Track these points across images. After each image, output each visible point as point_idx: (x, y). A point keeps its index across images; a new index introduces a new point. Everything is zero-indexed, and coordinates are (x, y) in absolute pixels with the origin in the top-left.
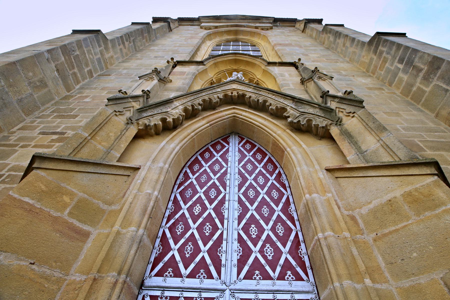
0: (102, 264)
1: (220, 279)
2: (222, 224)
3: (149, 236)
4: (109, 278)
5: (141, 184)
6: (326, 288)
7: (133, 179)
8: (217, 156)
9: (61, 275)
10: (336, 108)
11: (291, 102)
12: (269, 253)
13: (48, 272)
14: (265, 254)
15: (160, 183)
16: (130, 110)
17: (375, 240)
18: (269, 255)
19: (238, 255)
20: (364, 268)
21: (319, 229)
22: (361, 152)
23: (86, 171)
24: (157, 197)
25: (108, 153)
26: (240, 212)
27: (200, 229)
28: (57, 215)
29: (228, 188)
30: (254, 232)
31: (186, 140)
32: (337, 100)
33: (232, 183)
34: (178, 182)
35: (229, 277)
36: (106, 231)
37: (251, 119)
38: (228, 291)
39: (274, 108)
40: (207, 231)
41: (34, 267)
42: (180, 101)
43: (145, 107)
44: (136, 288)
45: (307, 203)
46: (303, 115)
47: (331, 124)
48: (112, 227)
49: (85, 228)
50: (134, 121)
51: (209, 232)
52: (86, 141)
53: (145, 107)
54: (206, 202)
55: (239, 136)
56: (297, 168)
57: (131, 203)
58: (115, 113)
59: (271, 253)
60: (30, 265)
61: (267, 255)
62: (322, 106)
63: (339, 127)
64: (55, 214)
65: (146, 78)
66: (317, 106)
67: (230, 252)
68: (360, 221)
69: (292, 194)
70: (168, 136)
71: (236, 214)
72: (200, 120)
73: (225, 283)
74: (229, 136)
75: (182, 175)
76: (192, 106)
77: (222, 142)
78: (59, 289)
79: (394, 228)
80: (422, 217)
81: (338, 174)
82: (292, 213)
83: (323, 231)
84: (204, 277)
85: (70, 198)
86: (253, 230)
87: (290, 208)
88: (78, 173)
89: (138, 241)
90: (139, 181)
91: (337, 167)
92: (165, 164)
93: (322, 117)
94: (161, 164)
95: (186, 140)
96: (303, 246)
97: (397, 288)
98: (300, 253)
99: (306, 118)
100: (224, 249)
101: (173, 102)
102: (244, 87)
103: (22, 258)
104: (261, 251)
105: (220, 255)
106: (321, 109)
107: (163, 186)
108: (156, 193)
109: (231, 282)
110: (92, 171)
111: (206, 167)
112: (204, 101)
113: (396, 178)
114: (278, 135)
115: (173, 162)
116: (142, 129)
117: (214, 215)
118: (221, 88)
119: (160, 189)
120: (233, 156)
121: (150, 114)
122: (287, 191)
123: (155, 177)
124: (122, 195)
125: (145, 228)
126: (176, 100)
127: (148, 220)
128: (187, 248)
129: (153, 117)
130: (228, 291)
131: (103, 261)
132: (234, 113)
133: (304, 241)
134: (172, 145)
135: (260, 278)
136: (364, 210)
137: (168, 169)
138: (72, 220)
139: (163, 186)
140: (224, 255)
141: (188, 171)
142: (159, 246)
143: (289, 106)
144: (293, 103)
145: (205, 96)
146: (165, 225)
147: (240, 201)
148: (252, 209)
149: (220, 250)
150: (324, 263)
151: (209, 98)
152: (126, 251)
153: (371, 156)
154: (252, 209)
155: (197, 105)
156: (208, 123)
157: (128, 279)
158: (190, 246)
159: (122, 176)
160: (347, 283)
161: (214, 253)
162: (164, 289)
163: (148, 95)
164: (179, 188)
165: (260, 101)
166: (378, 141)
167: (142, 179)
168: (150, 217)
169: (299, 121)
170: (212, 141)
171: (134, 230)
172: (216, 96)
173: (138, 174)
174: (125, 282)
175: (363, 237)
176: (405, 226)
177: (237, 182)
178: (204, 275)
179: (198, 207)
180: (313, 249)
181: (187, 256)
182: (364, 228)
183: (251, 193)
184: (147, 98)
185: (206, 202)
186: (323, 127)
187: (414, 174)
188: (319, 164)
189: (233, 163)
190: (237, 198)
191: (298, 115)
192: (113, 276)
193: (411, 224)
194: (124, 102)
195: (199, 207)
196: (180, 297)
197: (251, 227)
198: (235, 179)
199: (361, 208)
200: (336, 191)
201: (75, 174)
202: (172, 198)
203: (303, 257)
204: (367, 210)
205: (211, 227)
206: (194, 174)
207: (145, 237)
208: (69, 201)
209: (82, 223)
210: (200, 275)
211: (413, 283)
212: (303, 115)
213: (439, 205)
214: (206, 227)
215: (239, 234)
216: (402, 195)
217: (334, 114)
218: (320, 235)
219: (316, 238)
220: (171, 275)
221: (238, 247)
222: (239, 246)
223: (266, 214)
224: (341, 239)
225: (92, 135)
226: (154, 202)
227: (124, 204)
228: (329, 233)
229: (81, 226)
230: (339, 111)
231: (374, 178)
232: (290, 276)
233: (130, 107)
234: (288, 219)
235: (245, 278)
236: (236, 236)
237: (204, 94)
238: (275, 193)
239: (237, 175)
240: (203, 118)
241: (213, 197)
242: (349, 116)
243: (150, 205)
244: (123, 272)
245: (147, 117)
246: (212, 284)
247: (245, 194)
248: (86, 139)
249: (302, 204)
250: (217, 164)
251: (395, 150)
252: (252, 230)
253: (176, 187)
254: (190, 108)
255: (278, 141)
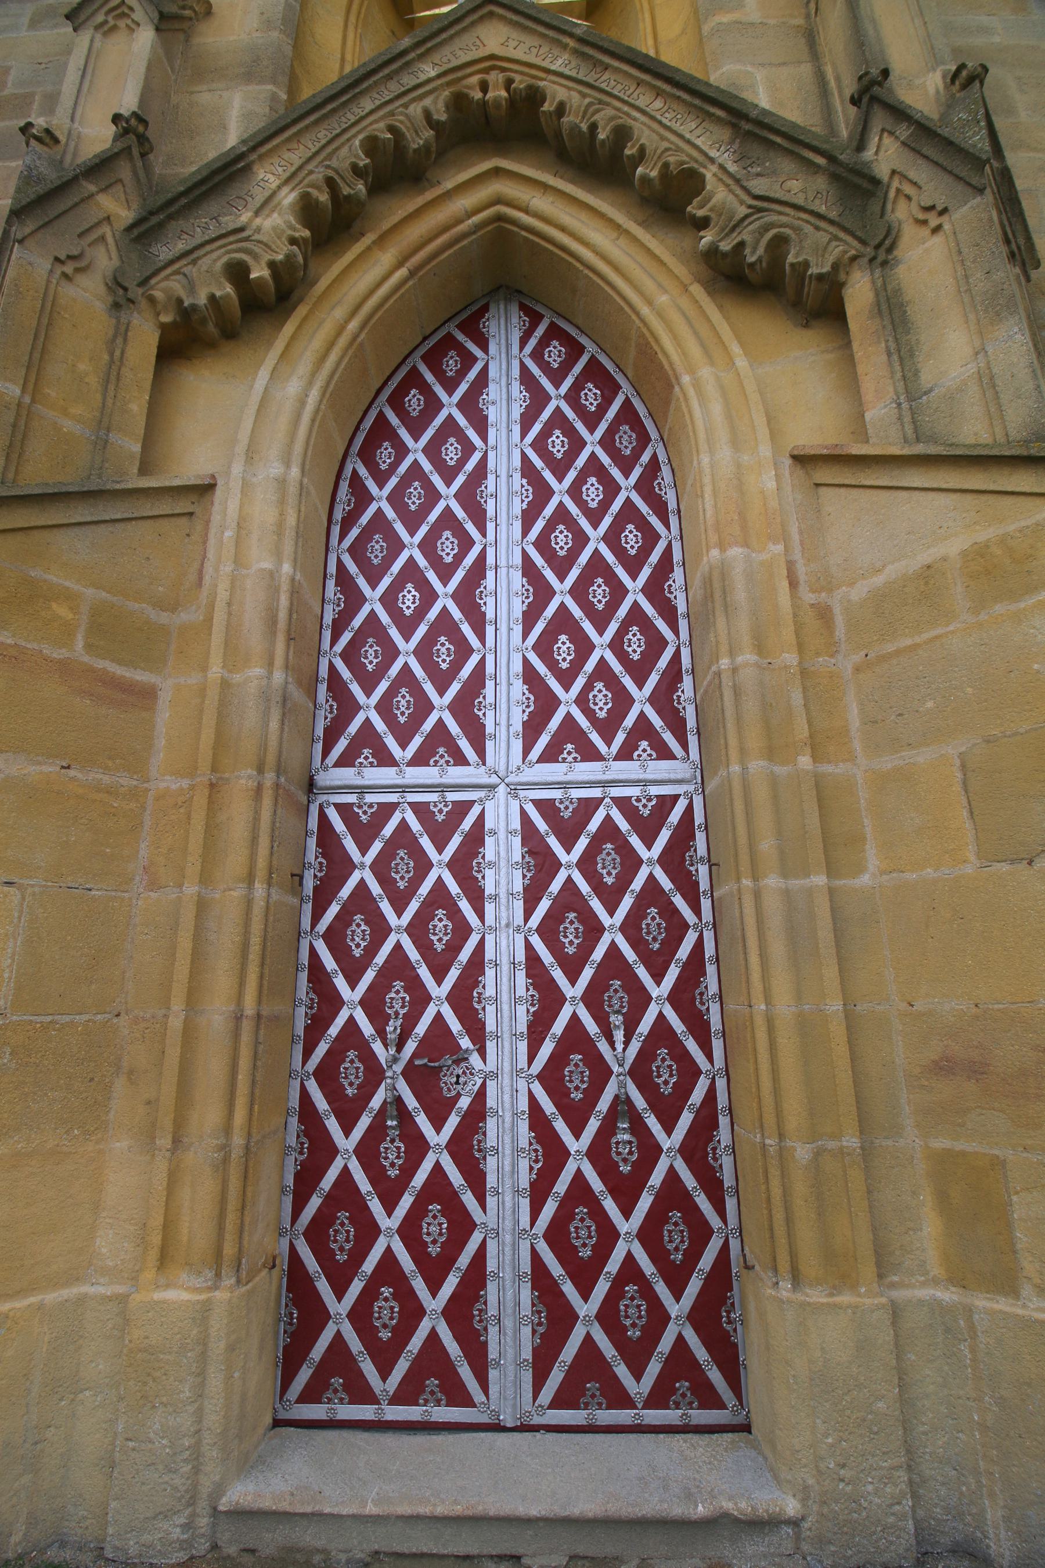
0: (214, 754)
1: (484, 764)
2: (482, 638)
3: (299, 683)
4: (243, 781)
5: (238, 542)
6: (715, 773)
7: (208, 522)
8: (450, 405)
9: (135, 783)
10: (894, 172)
11: (726, 134)
12: (601, 704)
13: (106, 779)
14: (592, 705)
15: (289, 535)
16: (102, 238)
17: (857, 670)
18: (601, 709)
19: (524, 711)
20: (806, 734)
21: (724, 648)
22: (911, 392)
23: (73, 521)
24: (293, 580)
25: (102, 444)
26: (527, 601)
27: (424, 652)
28: (61, 657)
29: (490, 526)
30: (564, 655)
31: (333, 358)
32: (904, 131)
33: (504, 509)
34: (338, 515)
35: (503, 760)
36: (194, 679)
37: (563, 229)
38: (502, 787)
39: (654, 174)
40: (444, 657)
41: (72, 773)
42: (276, 160)
43: (152, 213)
44: (300, 792)
45: (710, 573)
46: (760, 210)
47: (854, 259)
48: (205, 669)
49: (138, 678)
50: (135, 292)
51: (448, 659)
52: (24, 412)
53: (152, 213)
54: (432, 576)
55: (523, 307)
56: (702, 456)
57: (229, 604)
58: (59, 269)
59: (606, 704)
60: (63, 771)
61: (596, 708)
62: (840, 164)
63: (878, 272)
64: (60, 654)
65: (100, 18)
66: (821, 161)
67: (504, 706)
68: (839, 620)
69: (681, 538)
70: (270, 344)
71: (518, 608)
72: (369, 249)
73: (496, 773)
74: (485, 309)
75: (344, 487)
76: (330, 182)
77: (461, 337)
78: (143, 808)
79: (908, 642)
80: (983, 617)
81: (824, 475)
82: (672, 597)
83: (732, 654)
84: (447, 762)
85: (71, 609)
86: (564, 648)
87: (671, 582)
88: (55, 531)
89: (278, 699)
90: (228, 534)
91: (825, 452)
92: (288, 465)
93: (832, 222)
94: (276, 469)
95: (333, 358)
96: (687, 682)
97: (866, 771)
98: (679, 700)
99: (767, 228)
100: (490, 699)
101: (248, 169)
102: (535, 41)
103: (40, 758)
104: (582, 701)
105: (480, 714)
106: (835, 177)
107: (300, 544)
108: (287, 568)
109: (510, 769)
110: (89, 519)
111: (416, 451)
112: (371, 145)
113: (969, 497)
114: (660, 315)
115: (310, 453)
116: (174, 324)
117: (456, 614)
118: (436, 57)
119: (296, 553)
120: (504, 402)
121: (181, 246)
122: (668, 528)
123: (270, 516)
124: (192, 577)
125: (287, 667)
126: (261, 157)
127: (288, 646)
128: (398, 702)
129: (194, 262)
130: (502, 787)
131: (214, 748)
132: (499, 201)
133: (693, 670)
134: (293, 387)
135: (575, 758)
136: (858, 593)
137: (301, 484)
138: (101, 662)
139: (300, 544)
140: (490, 714)
141: (363, 472)
142: (327, 701)
143: (712, 160)
144: (731, 142)
145: (371, 117)
146: (331, 648)
147: (528, 568)
148: (562, 589)
149: (480, 703)
150: (721, 726)
151: (391, 129)
152: (257, 724)
153: (936, 411)
154: (562, 589)
155: (349, 175)
156: (400, 265)
157: (283, 780)
158: (404, 697)
159: (173, 520)
160: (757, 765)
161: (465, 708)
162: (362, 790)
163: (142, 139)
164: (342, 536)
165: (602, 136)
166: (977, 354)
167: (234, 525)
168: (290, 639)
169: (741, 244)
170: (425, 339)
171: (260, 676)
172: (416, 110)
173: (217, 508)
174: (277, 786)
175: (833, 661)
176: (936, 637)
177: (517, 501)
178: (447, 758)
179: (409, 592)
180: (706, 692)
181: (402, 720)
182: (843, 639)
183: (562, 540)
184: (143, 155)
185: (432, 576)
186: (820, 277)
187: (1018, 489)
188: (774, 435)
189: (504, 432)
190: (518, 560)
191: (743, 211)
192: (250, 777)
193: (953, 632)
194: (70, 203)
195: (414, 593)
196: (399, 803)
197: (556, 641)
198: (510, 494)
199: (852, 584)
200: (801, 532)
201: (46, 534)
202: (332, 569)
203: (684, 708)
204: (866, 589)
205: (452, 647)
206: (381, 480)
207: (292, 688)
208: (71, 616)
209: (126, 665)
210: (437, 758)
211: (902, 763)
212: (760, 210)
213: (1036, 588)
214: (439, 647)
215: (526, 662)
216: (964, 554)
217: (877, 209)
218: (725, 663)
219: (714, 668)
220: (371, 763)
221: (524, 694)
222: (527, 692)
223: (600, 601)
224: (774, 670)
225: (31, 386)
226: (288, 595)
227: (211, 606)
228: (747, 657)
229: (128, 675)
230: (898, 191)
231: (917, 493)
232: (644, 751)
233: (98, 224)
234: (660, 614)
235: (541, 760)
236: (518, 667)
237: (367, 104)
238: (631, 536)
239: (518, 480)
240: (381, 241)
241: (449, 560)
242: (925, 222)
243: (281, 607)
244: (267, 767)
245: (171, 262)
246: (468, 776)
247: (543, 544)
248: (19, 405)
249: (699, 574)
250: (452, 440)
251: (1004, 398)
252: (559, 648)
253: (336, 530)
254: (324, 197)
255: (657, 340)
